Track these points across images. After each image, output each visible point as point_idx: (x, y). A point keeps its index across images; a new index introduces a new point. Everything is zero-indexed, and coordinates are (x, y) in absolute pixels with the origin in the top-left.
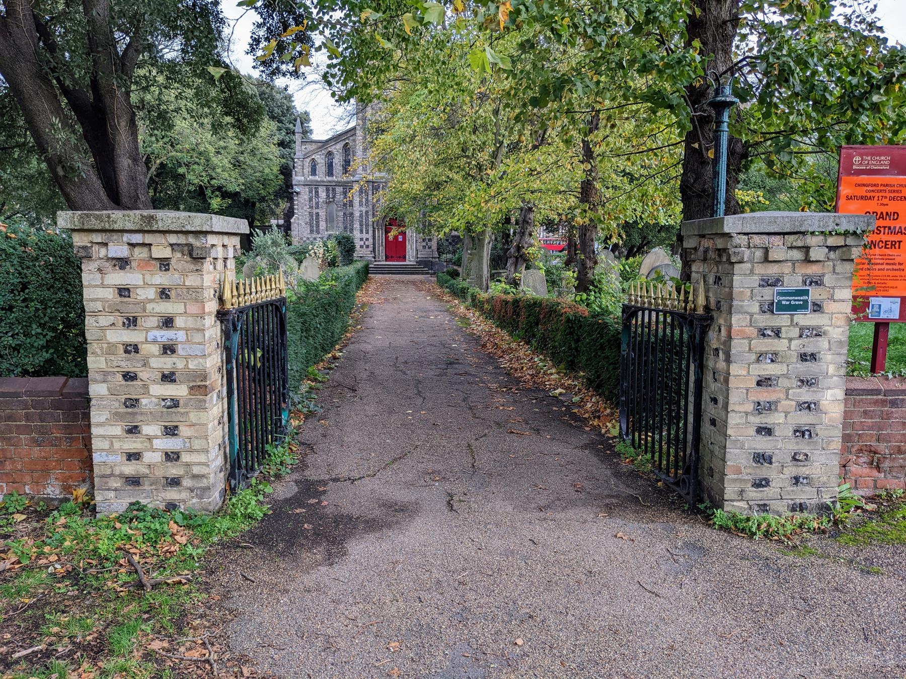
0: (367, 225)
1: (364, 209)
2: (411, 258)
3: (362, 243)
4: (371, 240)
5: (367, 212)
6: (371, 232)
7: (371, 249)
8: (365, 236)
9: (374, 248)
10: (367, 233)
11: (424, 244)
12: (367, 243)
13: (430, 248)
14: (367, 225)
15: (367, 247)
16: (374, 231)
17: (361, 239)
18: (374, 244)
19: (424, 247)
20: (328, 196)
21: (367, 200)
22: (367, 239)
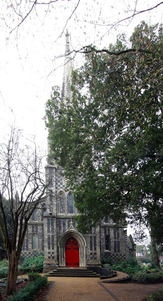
0: (53, 244)
1: (51, 234)
2: (83, 265)
4: (56, 254)
5: (53, 236)
6: (55, 248)
8: (51, 251)
9: (58, 259)
10: (53, 249)
11: (92, 256)
13: (95, 259)
14: (53, 244)
15: (53, 257)
16: (58, 248)
17: (49, 253)
18: (58, 256)
19: (92, 258)
20: (33, 231)
21: (53, 228)
22: (53, 253)
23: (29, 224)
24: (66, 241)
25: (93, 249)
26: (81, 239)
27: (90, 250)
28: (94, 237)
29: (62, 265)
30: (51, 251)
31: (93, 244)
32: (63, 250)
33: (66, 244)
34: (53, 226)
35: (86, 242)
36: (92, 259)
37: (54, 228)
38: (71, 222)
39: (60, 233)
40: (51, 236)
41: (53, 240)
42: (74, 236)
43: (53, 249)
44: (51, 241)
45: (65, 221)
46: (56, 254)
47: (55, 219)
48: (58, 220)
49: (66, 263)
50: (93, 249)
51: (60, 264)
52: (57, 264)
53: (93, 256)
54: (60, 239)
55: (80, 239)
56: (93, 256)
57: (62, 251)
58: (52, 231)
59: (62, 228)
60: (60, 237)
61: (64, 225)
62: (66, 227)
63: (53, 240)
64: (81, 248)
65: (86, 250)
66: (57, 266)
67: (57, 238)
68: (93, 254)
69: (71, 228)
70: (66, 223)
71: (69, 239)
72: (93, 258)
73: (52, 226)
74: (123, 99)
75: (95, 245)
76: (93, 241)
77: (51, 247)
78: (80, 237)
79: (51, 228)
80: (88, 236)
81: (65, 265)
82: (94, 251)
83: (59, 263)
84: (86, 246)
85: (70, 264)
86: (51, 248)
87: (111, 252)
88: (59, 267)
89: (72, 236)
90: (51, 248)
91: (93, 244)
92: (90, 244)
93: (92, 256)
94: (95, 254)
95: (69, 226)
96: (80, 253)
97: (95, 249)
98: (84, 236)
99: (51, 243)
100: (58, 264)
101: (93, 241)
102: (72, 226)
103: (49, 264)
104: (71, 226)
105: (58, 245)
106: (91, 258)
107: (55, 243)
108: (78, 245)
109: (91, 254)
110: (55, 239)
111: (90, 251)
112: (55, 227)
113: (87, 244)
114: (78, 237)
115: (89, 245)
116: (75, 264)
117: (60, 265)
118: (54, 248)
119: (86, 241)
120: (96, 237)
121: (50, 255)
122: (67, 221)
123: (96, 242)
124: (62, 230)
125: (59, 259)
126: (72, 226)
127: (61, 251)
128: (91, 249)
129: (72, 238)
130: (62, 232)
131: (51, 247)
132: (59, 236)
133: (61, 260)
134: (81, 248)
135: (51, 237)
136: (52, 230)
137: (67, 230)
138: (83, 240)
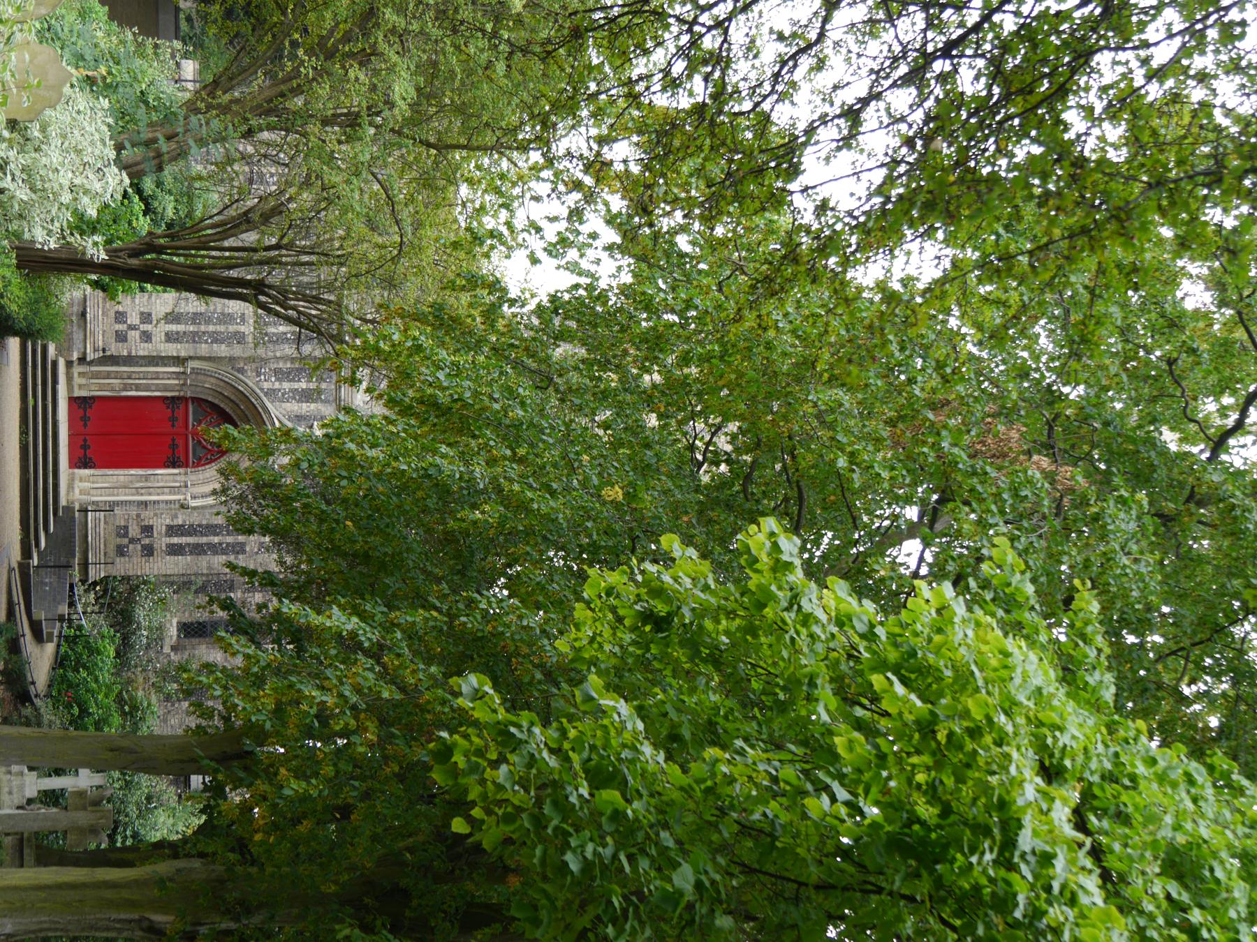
0: (195, 338)
2: (80, 486)
3: (134, 319)
4: (143, 350)
5: (240, 338)
6: (172, 349)
7: (115, 349)
8: (159, 331)
10: (170, 337)
11: (134, 531)
12: (134, 335)
13: (121, 551)
14: (195, 338)
15: (121, 337)
16: (179, 361)
17: (146, 317)
18: (130, 360)
19: (123, 531)
22: (147, 337)
25: (175, 540)
27: (168, 522)
28: (243, 545)
29: (77, 380)
30: (159, 331)
31: (204, 540)
32: (166, 388)
33: (198, 401)
36: (119, 535)
39: (259, 374)
40: (242, 329)
41: (216, 338)
43: (170, 337)
44: (211, 328)
45: (326, 402)
46: (141, 353)
49: (93, 398)
50: (175, 540)
51: (82, 369)
53: (132, 541)
54: (225, 372)
56: (132, 541)
57: (159, 383)
59: (286, 386)
61: (306, 396)
62: (294, 407)
63: (215, 341)
64: (183, 478)
66: (75, 356)
67: (232, 359)
68: (147, 541)
70: (313, 406)
72: (126, 541)
75: (198, 550)
76: (216, 540)
77: (180, 328)
81: (77, 393)
82: (162, 542)
83: (91, 363)
84: (193, 503)
85: (84, 419)
86: (173, 327)
87: (167, 650)
88: (69, 364)
90: (173, 327)
91: (204, 540)
93: (134, 531)
94: (149, 551)
96: (150, 472)
97: (175, 550)
99: (203, 328)
100: (82, 360)
101: (216, 540)
103: (84, 314)
105: (192, 364)
106: (126, 527)
107: (203, 349)
109: (148, 530)
110: (222, 350)
111: (160, 523)
115: (195, 519)
116: (85, 447)
117: (77, 370)
118: (177, 340)
120: (244, 552)
121: (134, 319)
123: (215, 553)
124: (277, 385)
125: (118, 364)
127: (157, 376)
128: (172, 530)
130: (266, 385)
131: (180, 328)
132: (241, 371)
133: (108, 375)
135: (232, 328)
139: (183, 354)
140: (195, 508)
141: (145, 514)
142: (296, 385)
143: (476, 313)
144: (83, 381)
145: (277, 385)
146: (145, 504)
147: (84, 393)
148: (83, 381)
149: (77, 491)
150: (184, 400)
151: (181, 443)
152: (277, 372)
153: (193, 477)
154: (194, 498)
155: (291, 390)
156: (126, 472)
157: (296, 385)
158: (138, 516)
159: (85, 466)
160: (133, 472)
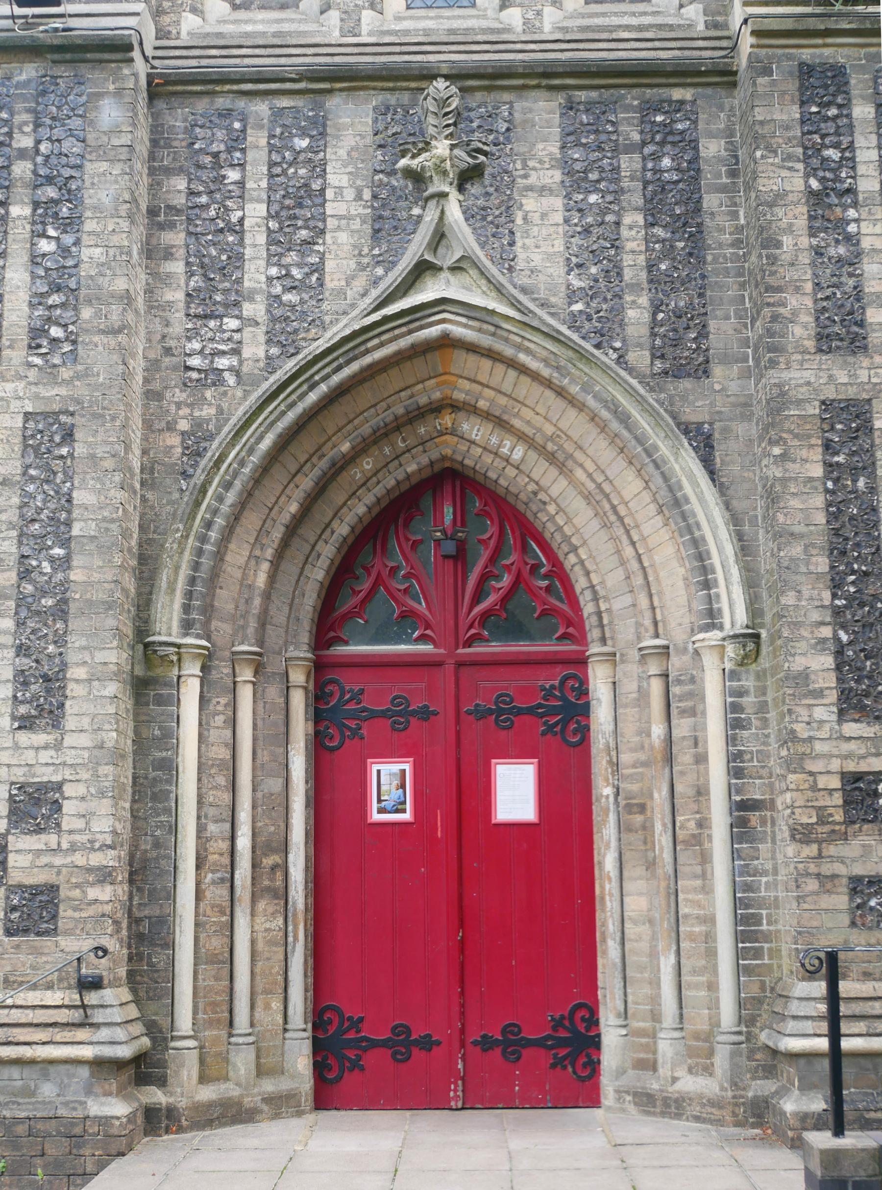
4: (94, 817)
6: (95, 703)
7: (90, 928)
16: (148, 684)
18: (145, 872)
23: (8, 681)
24: (328, 551)
26: (629, 485)
27: (825, 712)
33: (327, 627)
34: (71, 224)
35: (745, 548)
37: (91, 254)
38: (441, 148)
42: (475, 429)
45: (319, 130)
47: (114, 112)
48: (177, 118)
49: (319, 1017)
52: (102, 1066)
55: (600, 498)
58: (37, 333)
59: (256, 272)
60: (214, 448)
61: (298, 208)
63: (60, 528)
65: (735, 723)
69: (422, 269)
70: (337, 177)
71: (397, 512)
73: (45, 213)
74: (570, 199)
78: (601, 450)
79: (35, 259)
80: (780, 401)
83: (159, 1034)
84: (735, 614)
85: (403, 1044)
89: (448, 447)
92: (836, 586)
95: (385, 225)
98: (696, 411)
102: (439, 237)
104: (431, 215)
105: (167, 624)
108: (573, 626)
110: (98, 501)
112: (106, 241)
113: (751, 583)
114: (559, 462)
116: (512, 1045)
119: (735, 519)
122: (353, 121)
124: (255, 309)
126: (439, 237)
127: (221, 770)
129: (452, 480)
130: (255, 348)
132: (195, 443)
134: (629, 687)
136: (37, 300)
137: (349, 285)
138: (674, 505)
139: (114, 656)
140: (754, 611)
141: (790, 802)
142: (256, 240)
143: (267, 955)
144: (242, 1062)
145: (255, 309)
146: (745, 812)
147: (301, 1061)
148: (242, 1062)
149: (690, 1084)
150: (322, 669)
151: (487, 690)
152: (206, 307)
153: (624, 632)
154: (711, 618)
155: (272, 259)
156: (606, 885)
157: (256, 240)
158: (802, 835)
159: (592, 1043)
160: (607, 861)
